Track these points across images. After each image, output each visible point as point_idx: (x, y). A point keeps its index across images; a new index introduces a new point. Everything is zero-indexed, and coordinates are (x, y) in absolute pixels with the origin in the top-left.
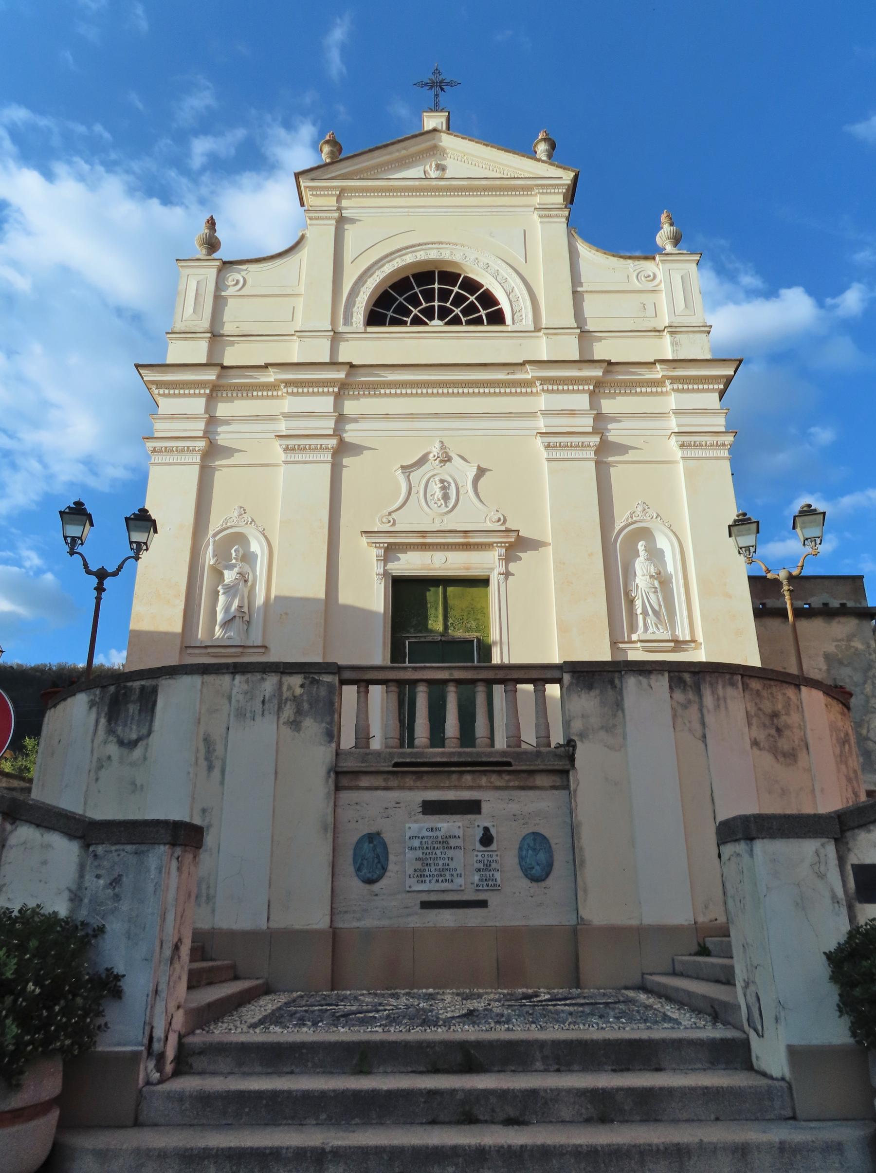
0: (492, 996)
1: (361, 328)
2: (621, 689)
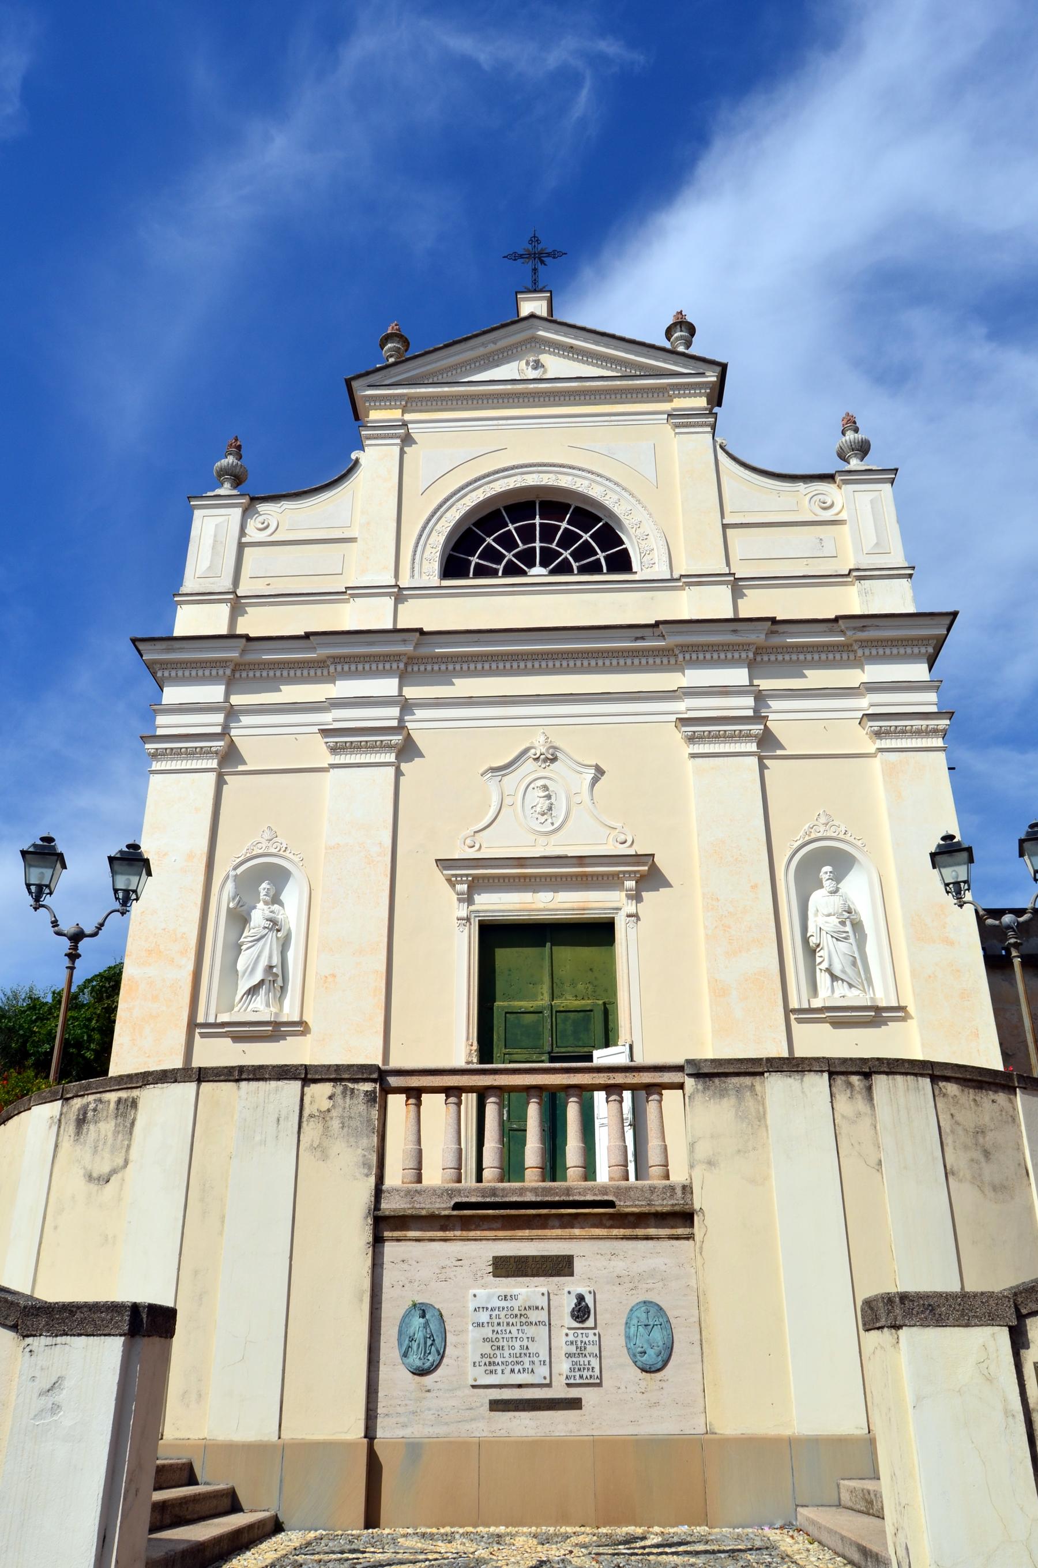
0: (581, 1539)
1: (435, 580)
2: (763, 1099)
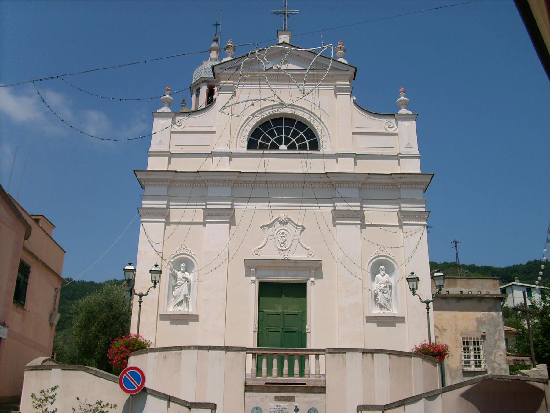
1: (244, 150)
